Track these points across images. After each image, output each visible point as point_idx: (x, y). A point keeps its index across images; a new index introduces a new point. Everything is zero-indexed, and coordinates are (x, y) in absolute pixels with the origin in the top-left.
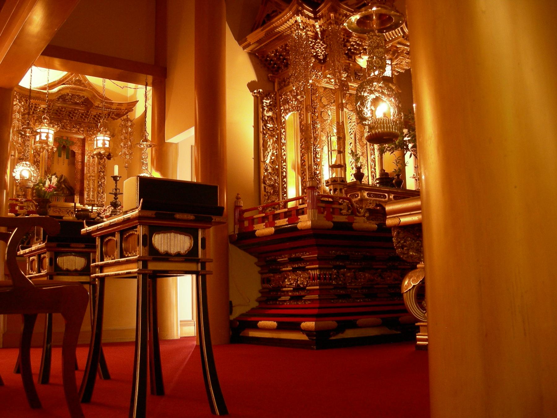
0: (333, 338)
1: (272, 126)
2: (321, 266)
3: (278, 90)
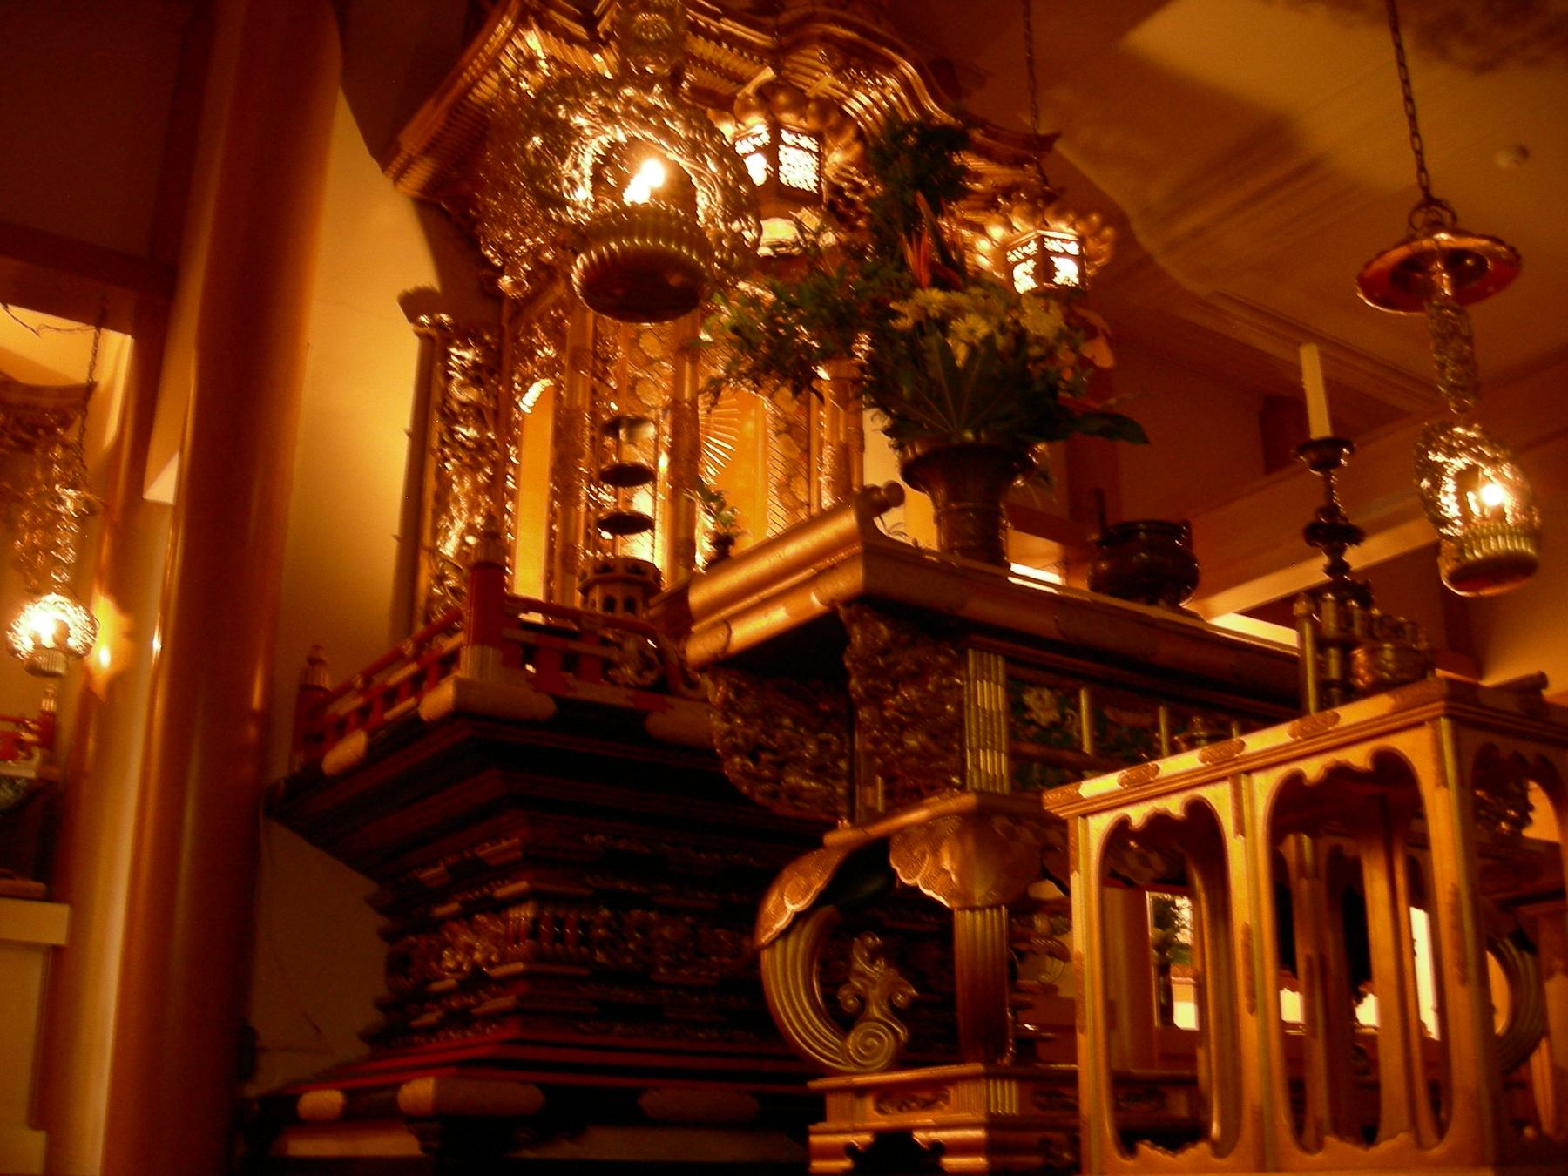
0: (528, 1154)
1: (472, 433)
3: (510, 321)
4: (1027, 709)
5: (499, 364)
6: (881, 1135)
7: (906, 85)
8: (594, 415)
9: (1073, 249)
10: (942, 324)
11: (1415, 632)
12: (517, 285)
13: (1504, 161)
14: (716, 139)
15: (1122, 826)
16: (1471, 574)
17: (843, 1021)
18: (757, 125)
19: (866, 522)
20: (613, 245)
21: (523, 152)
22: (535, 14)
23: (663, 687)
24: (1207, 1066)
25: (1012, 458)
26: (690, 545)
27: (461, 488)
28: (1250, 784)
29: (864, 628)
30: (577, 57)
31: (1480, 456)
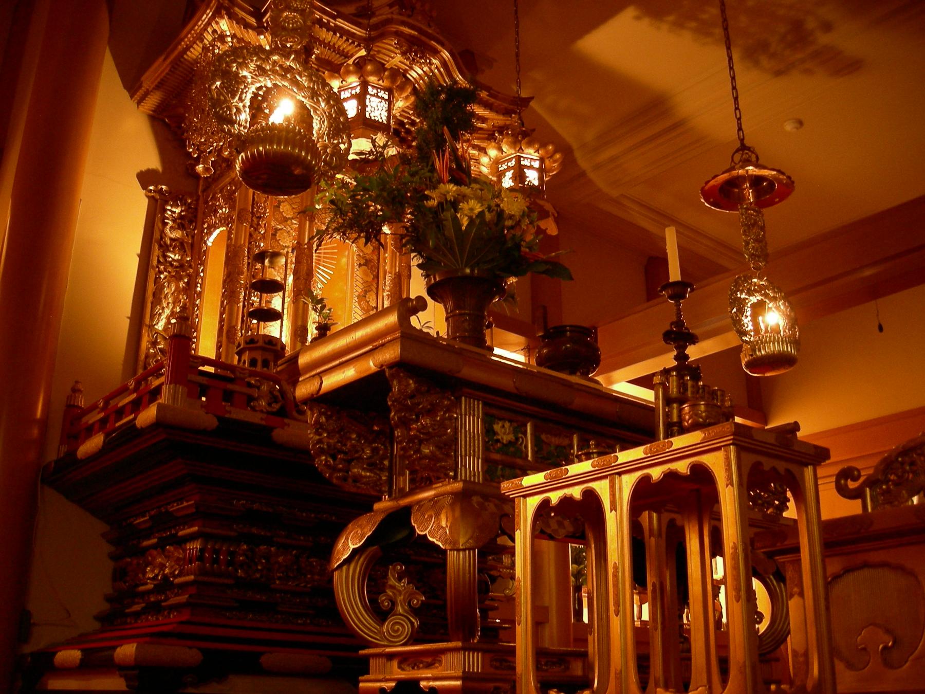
1: (177, 257)
2: (208, 530)
3: (203, 191)
4: (495, 433)
5: (196, 217)
6: (401, 683)
7: (444, 64)
8: (249, 249)
9: (536, 164)
10: (454, 204)
11: (723, 395)
12: (207, 170)
13: (789, 127)
14: (327, 88)
15: (546, 503)
16: (756, 364)
17: (381, 614)
18: (353, 80)
19: (404, 320)
20: (261, 148)
21: (210, 89)
22: (225, 9)
23: (283, 413)
24: (593, 647)
25: (494, 285)
26: (305, 330)
27: (169, 290)
28: (620, 482)
29: (400, 383)
30: (250, 36)
31: (766, 295)
